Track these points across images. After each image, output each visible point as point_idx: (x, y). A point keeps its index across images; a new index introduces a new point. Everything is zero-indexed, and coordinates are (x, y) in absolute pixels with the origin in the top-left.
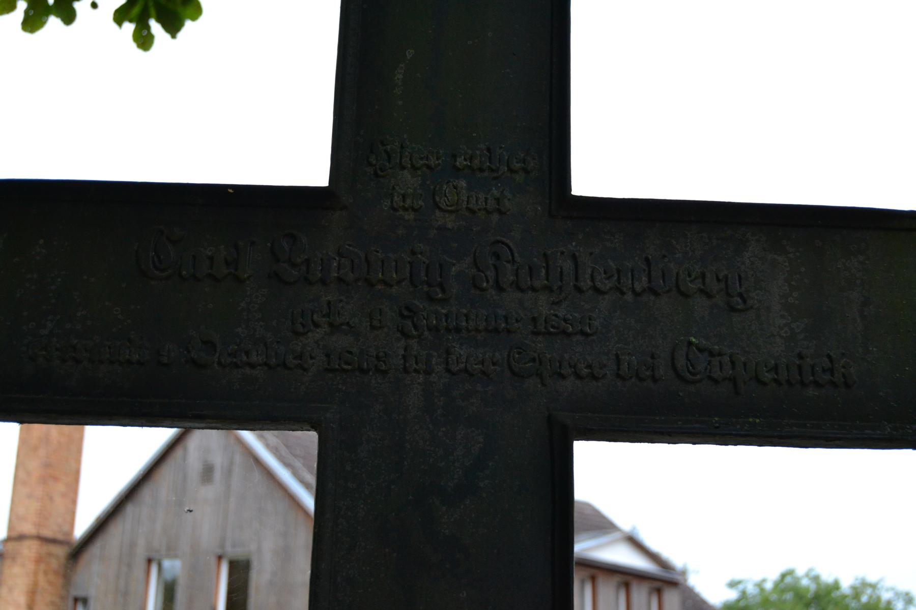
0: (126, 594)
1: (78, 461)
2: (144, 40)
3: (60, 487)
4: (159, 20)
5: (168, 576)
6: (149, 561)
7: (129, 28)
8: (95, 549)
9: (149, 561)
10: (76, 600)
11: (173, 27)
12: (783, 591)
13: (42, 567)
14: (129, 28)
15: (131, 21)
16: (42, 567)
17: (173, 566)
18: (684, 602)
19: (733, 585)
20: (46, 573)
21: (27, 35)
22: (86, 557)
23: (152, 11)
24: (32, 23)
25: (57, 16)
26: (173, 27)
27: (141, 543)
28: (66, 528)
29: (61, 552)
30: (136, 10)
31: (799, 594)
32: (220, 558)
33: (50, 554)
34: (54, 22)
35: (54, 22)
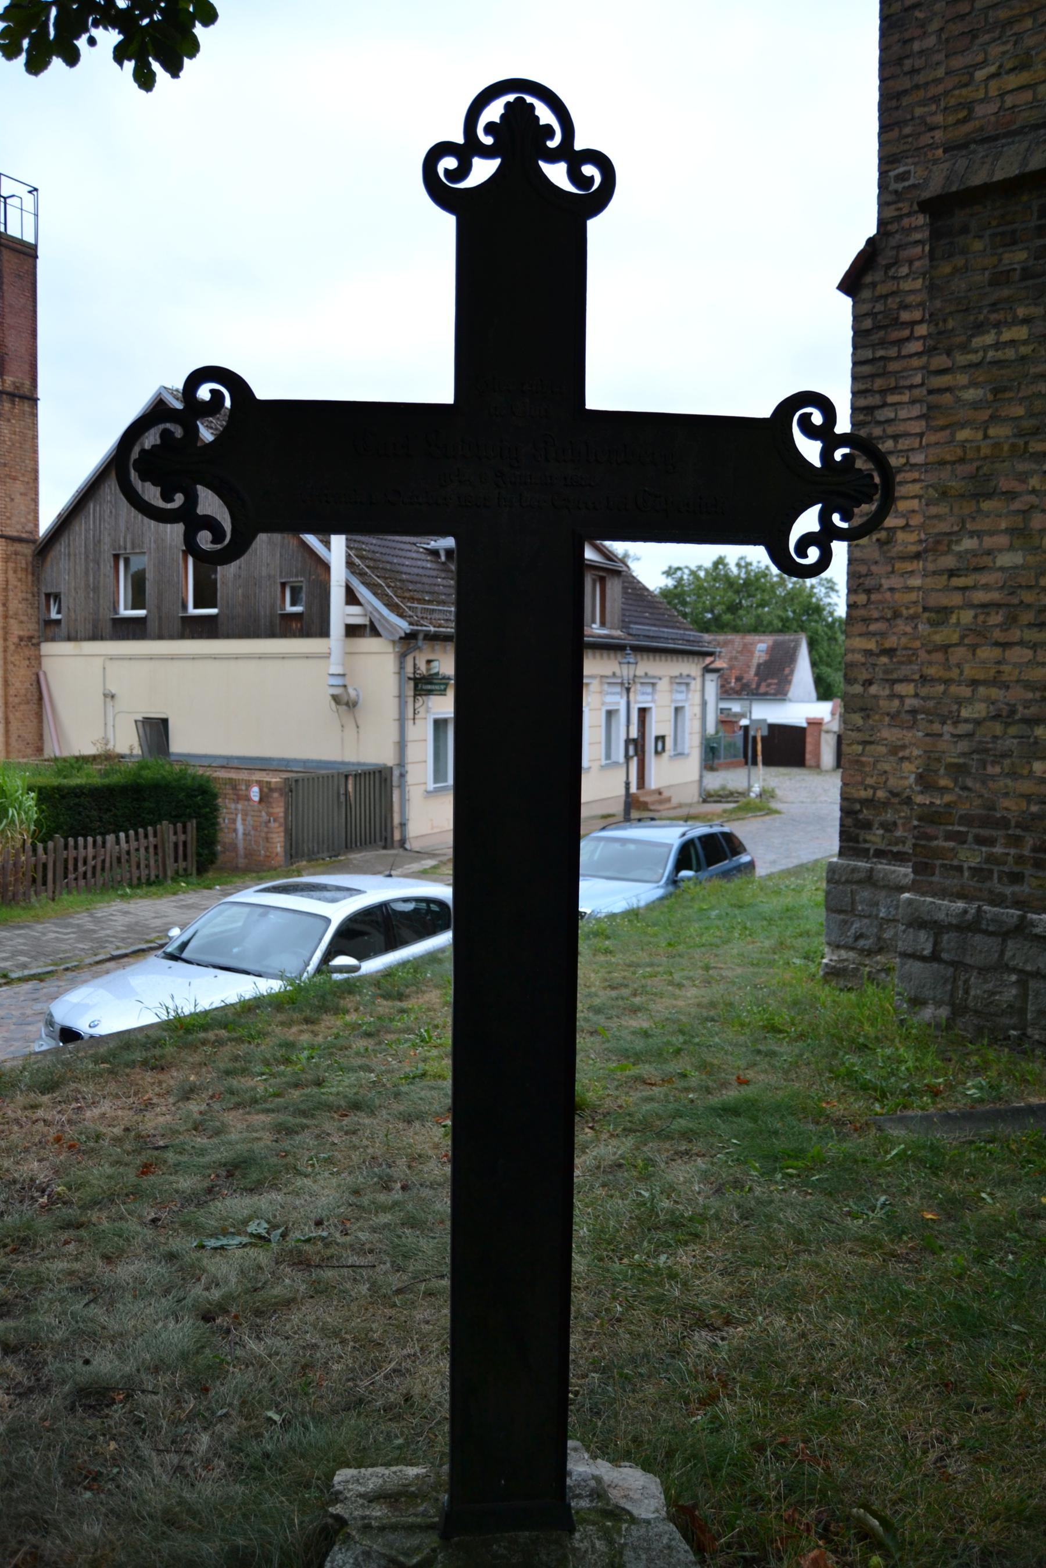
0: (96, 589)
1: (35, 461)
2: (145, 80)
3: (19, 486)
4: (156, 59)
5: (134, 568)
6: (116, 557)
7: (130, 65)
8: (61, 547)
9: (116, 557)
10: (48, 596)
11: (174, 69)
12: (715, 580)
13: (11, 565)
14: (130, 65)
15: (129, 60)
16: (11, 565)
17: (137, 563)
18: (625, 589)
19: (669, 573)
20: (15, 572)
21: (32, 78)
22: (53, 554)
23: (150, 48)
24: (36, 66)
25: (58, 56)
26: (174, 69)
27: (107, 540)
28: (30, 527)
29: (27, 550)
30: (133, 48)
31: (730, 582)
32: (283, 585)
33: (16, 553)
34: (57, 63)
35: (57, 63)
